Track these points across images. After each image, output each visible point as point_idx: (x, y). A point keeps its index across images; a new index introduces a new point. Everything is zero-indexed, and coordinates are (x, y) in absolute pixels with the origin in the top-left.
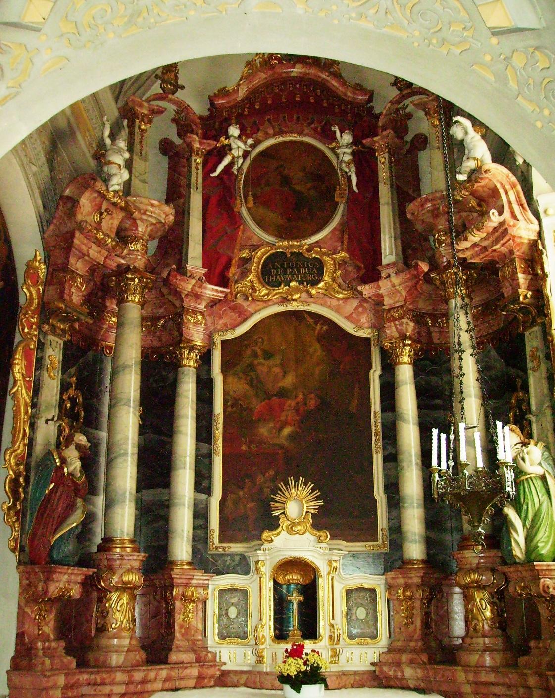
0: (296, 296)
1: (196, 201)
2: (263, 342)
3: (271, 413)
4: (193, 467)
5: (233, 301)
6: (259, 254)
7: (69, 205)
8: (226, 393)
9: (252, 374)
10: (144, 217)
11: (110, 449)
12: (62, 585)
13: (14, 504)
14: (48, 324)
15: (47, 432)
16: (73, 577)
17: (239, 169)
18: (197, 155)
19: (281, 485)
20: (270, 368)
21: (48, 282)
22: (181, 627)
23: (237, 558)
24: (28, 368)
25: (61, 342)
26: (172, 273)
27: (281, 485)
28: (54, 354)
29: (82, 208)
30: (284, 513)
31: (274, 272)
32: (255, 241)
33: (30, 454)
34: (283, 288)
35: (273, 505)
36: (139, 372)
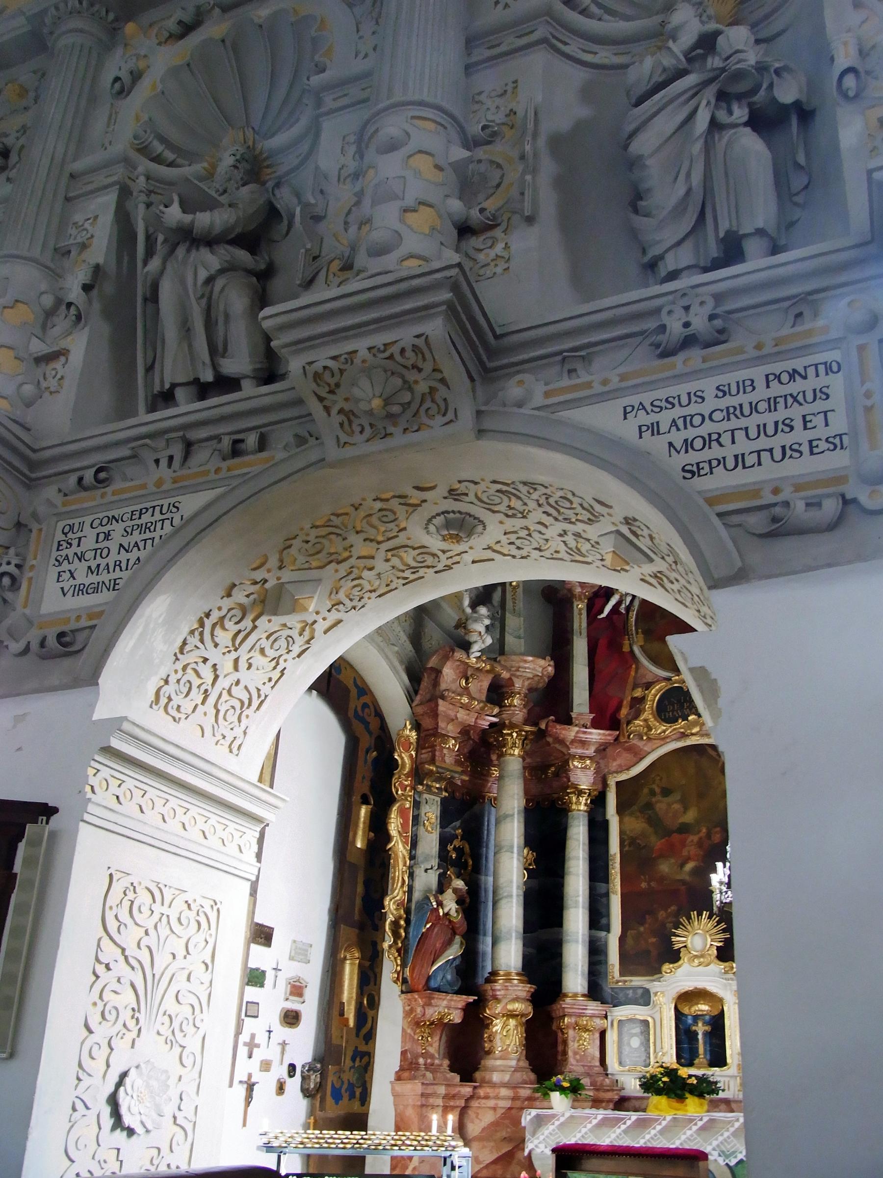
0: (695, 730)
1: (580, 647)
2: (661, 780)
3: (671, 851)
4: (587, 905)
5: (626, 742)
6: (653, 691)
7: (433, 676)
8: (622, 833)
9: (650, 812)
10: (518, 673)
11: (495, 892)
12: (441, 1009)
13: (395, 942)
14: (422, 784)
15: (426, 879)
16: (453, 1003)
17: (628, 609)
18: (580, 599)
19: (683, 920)
20: (669, 805)
21: (420, 747)
22: (575, 1053)
23: (640, 991)
24: (404, 825)
25: (439, 799)
26: (551, 724)
27: (683, 920)
28: (431, 812)
29: (446, 677)
30: (685, 946)
31: (669, 708)
32: (649, 678)
33: (410, 900)
34: (681, 723)
35: (674, 939)
36: (522, 820)
